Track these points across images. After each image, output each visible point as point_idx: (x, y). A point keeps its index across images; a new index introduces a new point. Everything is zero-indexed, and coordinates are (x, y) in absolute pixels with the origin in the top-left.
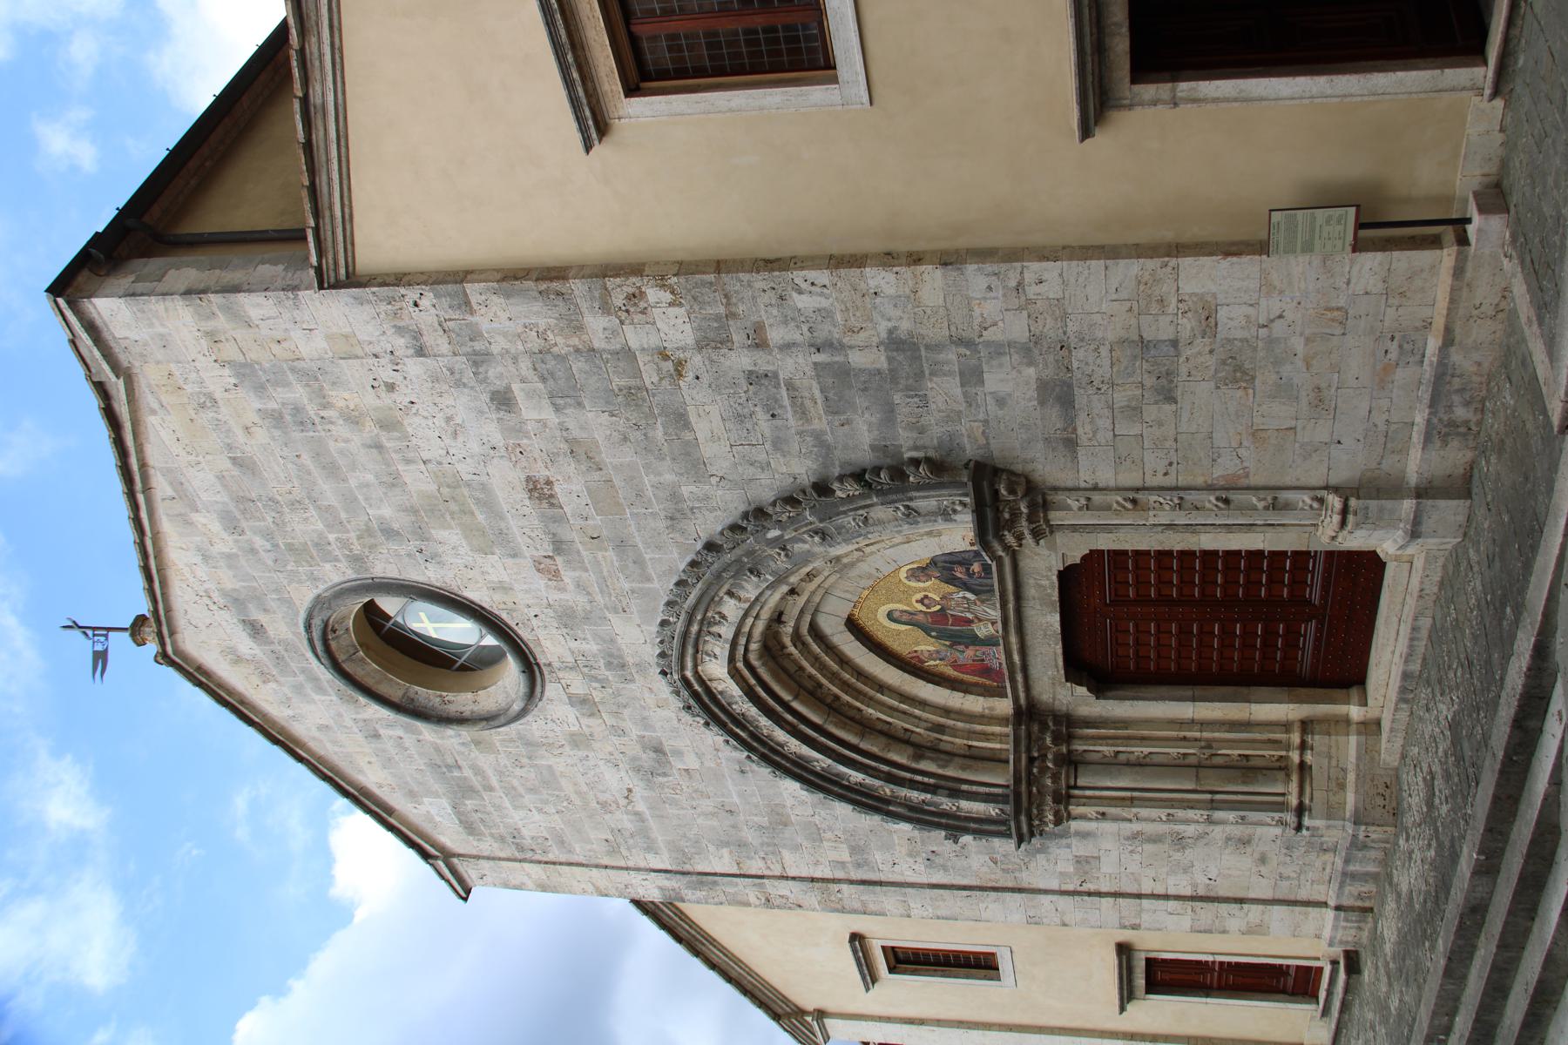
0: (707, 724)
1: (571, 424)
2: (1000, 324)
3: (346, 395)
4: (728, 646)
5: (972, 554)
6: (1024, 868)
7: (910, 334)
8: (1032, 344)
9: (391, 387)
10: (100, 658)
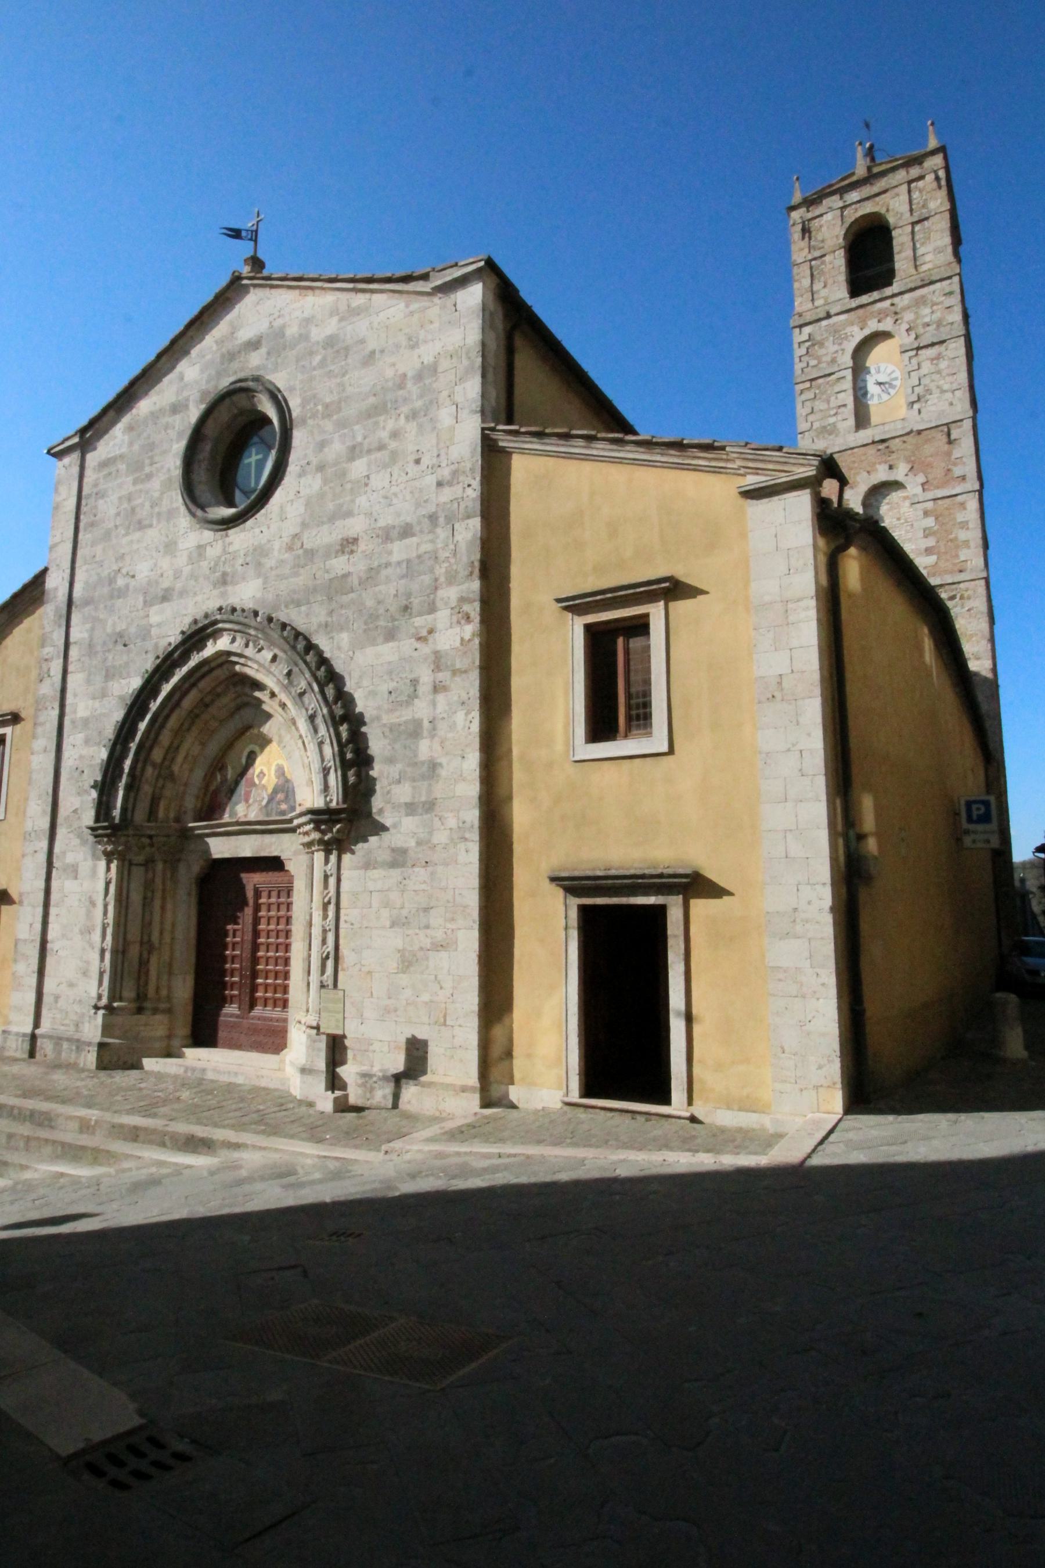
0: (183, 633)
1: (389, 571)
2: (443, 828)
3: (414, 433)
4: (239, 651)
5: (293, 805)
6: (69, 830)
7: (439, 776)
8: (430, 845)
9: (418, 462)
10: (236, 234)
